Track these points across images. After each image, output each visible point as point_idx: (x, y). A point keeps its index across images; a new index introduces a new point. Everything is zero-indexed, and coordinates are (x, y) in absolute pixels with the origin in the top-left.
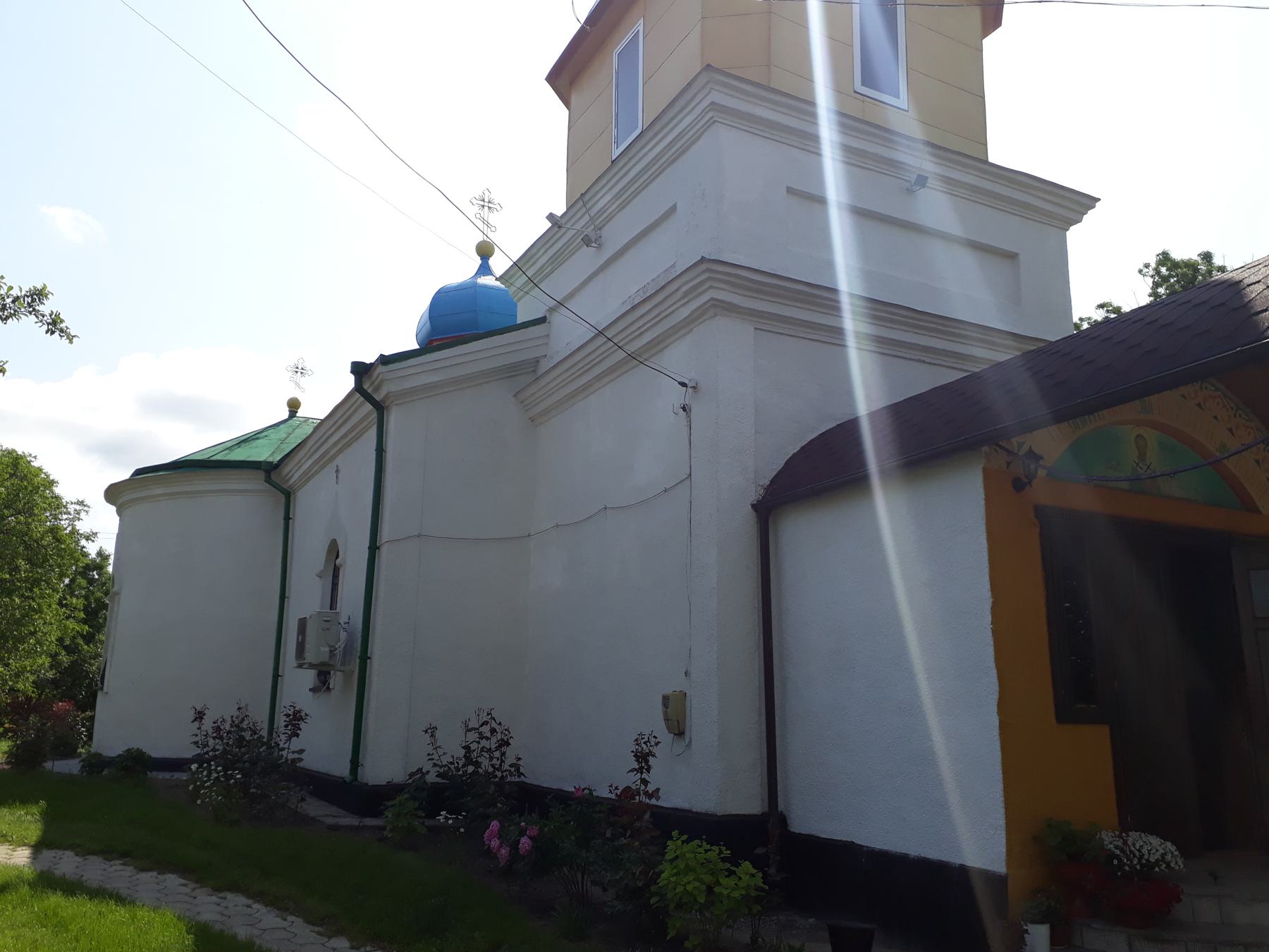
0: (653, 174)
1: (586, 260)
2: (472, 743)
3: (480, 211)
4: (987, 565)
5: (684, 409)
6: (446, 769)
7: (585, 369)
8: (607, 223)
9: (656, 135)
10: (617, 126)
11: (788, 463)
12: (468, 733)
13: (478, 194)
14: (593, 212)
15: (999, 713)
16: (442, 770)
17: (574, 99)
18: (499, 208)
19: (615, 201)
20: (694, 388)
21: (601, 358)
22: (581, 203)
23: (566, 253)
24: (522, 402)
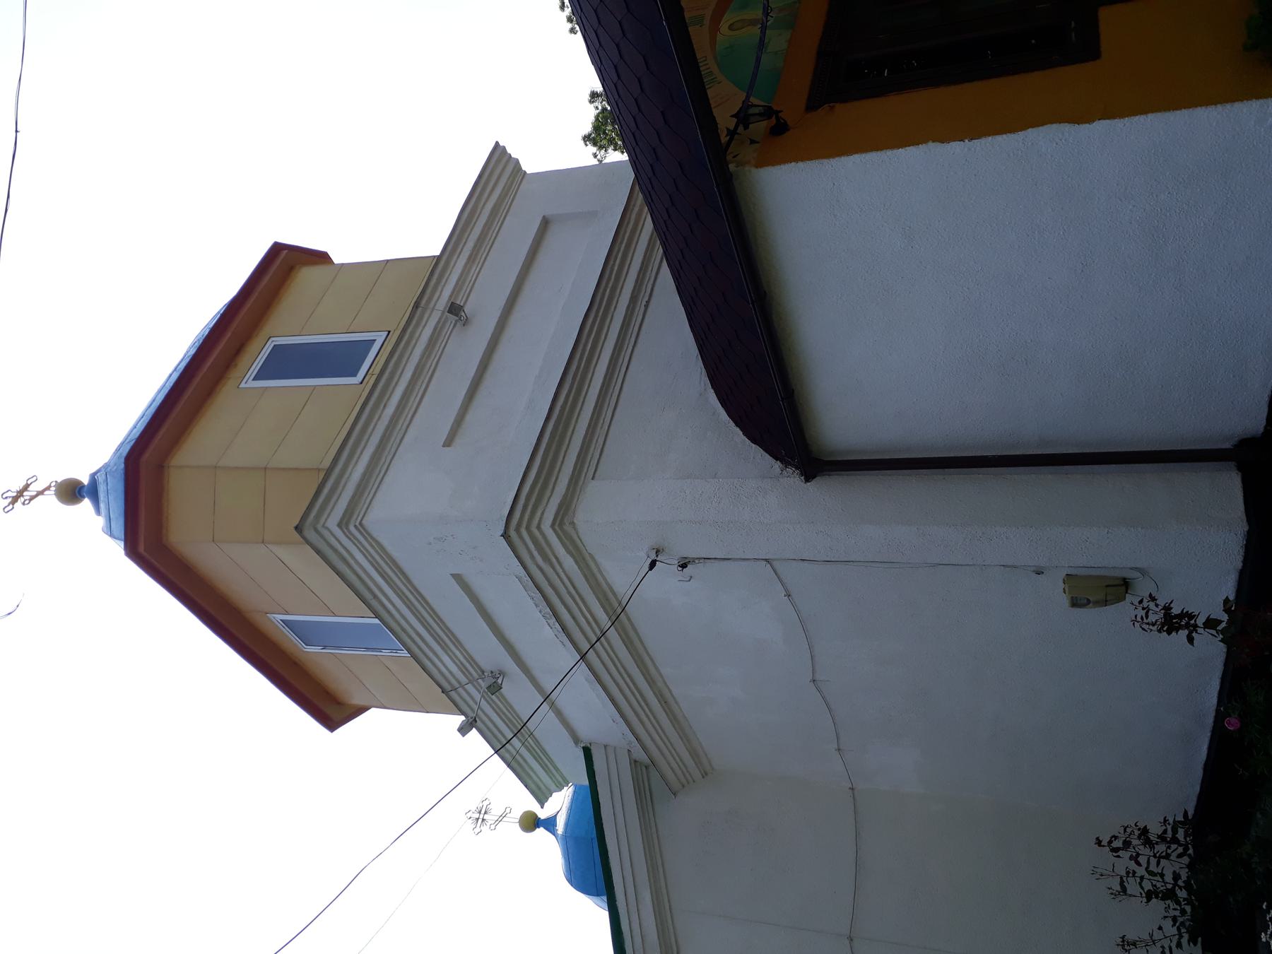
0: (417, 599)
1: (520, 696)
2: (1142, 888)
3: (488, 824)
4: (883, 152)
5: (684, 566)
6: (1183, 930)
7: (640, 699)
8: (476, 664)
9: (375, 596)
10: (380, 650)
11: (754, 440)
12: (1129, 892)
13: (470, 825)
14: (464, 680)
15: (1089, 120)
16: (1186, 936)
17: (357, 701)
18: (487, 802)
19: (452, 651)
20: (658, 552)
21: (625, 676)
22: (453, 694)
23: (511, 717)
24: (683, 786)
